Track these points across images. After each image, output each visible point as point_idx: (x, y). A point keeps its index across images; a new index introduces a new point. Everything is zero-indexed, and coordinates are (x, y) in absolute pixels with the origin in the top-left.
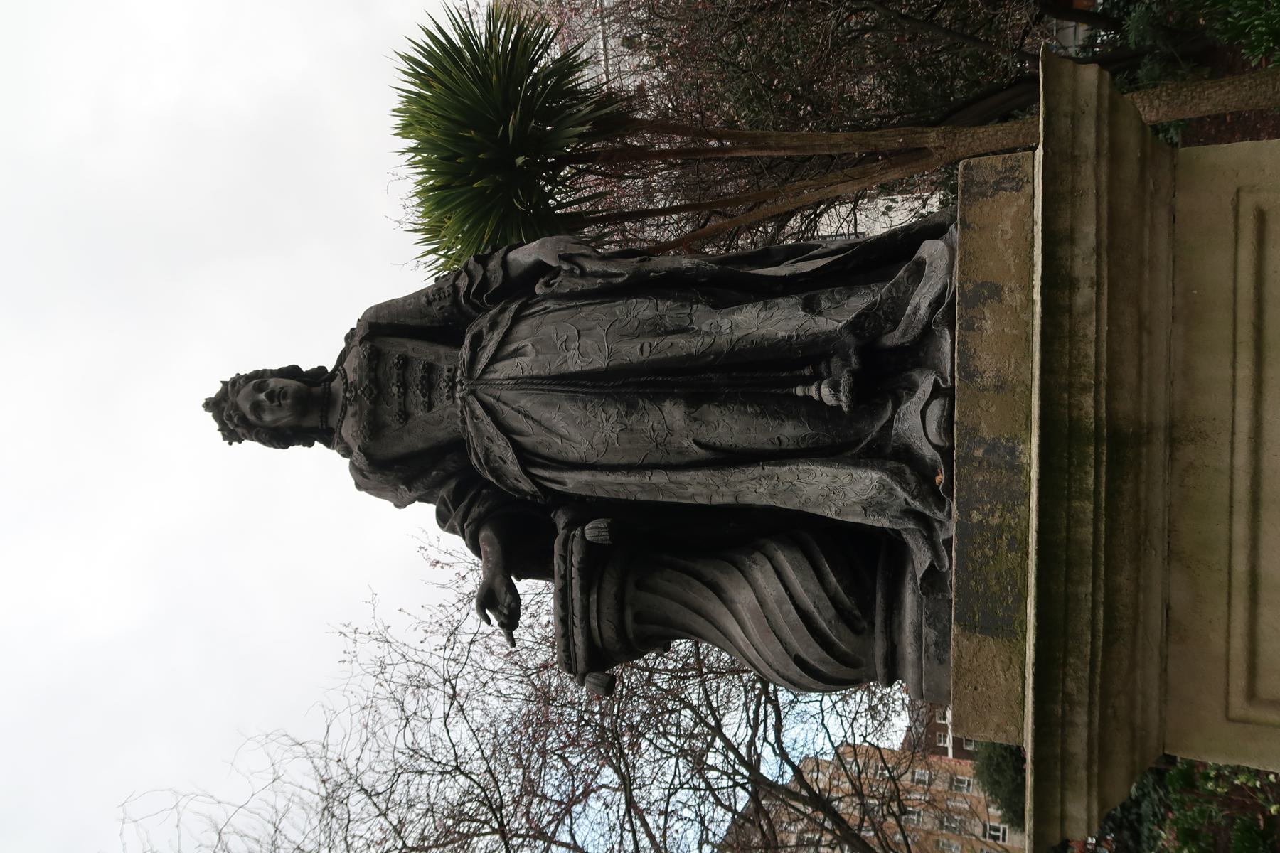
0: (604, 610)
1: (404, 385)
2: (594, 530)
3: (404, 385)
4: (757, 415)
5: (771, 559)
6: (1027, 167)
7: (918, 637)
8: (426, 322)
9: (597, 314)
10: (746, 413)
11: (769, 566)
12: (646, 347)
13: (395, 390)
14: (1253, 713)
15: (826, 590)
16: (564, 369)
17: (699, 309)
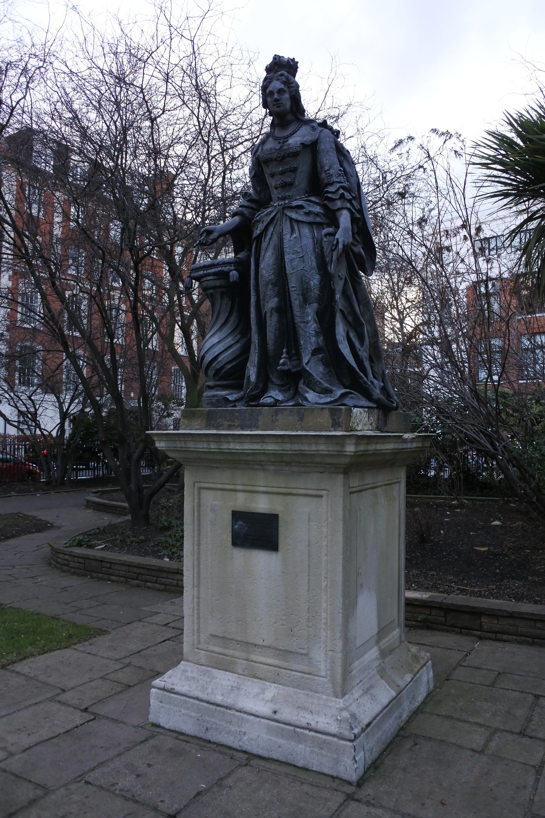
0: (210, 282)
1: (282, 173)
2: (234, 275)
3: (282, 173)
4: (275, 335)
6: (340, 429)
7: (214, 396)
8: (319, 170)
9: (312, 261)
11: (233, 342)
12: (295, 289)
13: (281, 169)
14: (196, 488)
16: (286, 254)
17: (315, 306)
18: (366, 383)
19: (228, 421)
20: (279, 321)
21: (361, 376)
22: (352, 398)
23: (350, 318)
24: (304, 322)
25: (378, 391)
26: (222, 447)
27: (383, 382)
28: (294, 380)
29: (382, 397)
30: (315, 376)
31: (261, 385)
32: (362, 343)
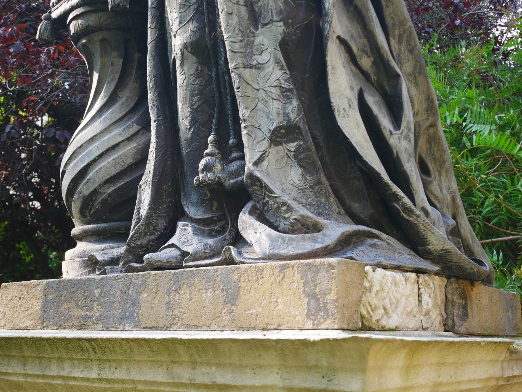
5: (129, 139)
10: (192, 96)
11: (120, 139)
15: (101, 186)
17: (279, 29)
18: (409, 211)
19: (81, 308)
20: (198, 74)
21: (395, 195)
22: (374, 246)
23: (366, 62)
24: (251, 67)
25: (442, 232)
26: (47, 372)
27: (454, 217)
28: (230, 202)
29: (450, 246)
30: (278, 192)
31: (162, 224)
32: (396, 118)
